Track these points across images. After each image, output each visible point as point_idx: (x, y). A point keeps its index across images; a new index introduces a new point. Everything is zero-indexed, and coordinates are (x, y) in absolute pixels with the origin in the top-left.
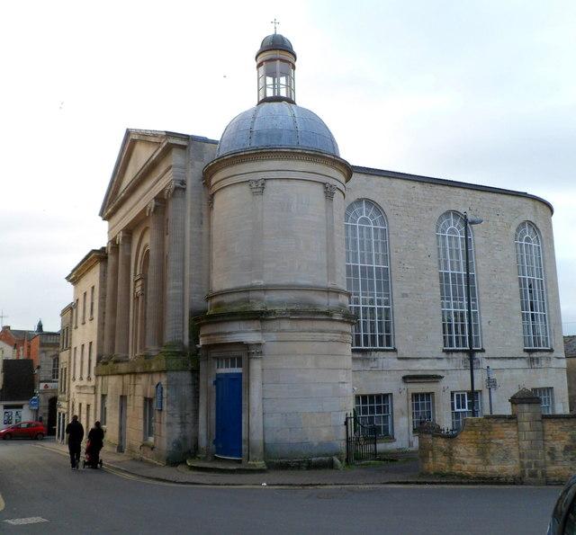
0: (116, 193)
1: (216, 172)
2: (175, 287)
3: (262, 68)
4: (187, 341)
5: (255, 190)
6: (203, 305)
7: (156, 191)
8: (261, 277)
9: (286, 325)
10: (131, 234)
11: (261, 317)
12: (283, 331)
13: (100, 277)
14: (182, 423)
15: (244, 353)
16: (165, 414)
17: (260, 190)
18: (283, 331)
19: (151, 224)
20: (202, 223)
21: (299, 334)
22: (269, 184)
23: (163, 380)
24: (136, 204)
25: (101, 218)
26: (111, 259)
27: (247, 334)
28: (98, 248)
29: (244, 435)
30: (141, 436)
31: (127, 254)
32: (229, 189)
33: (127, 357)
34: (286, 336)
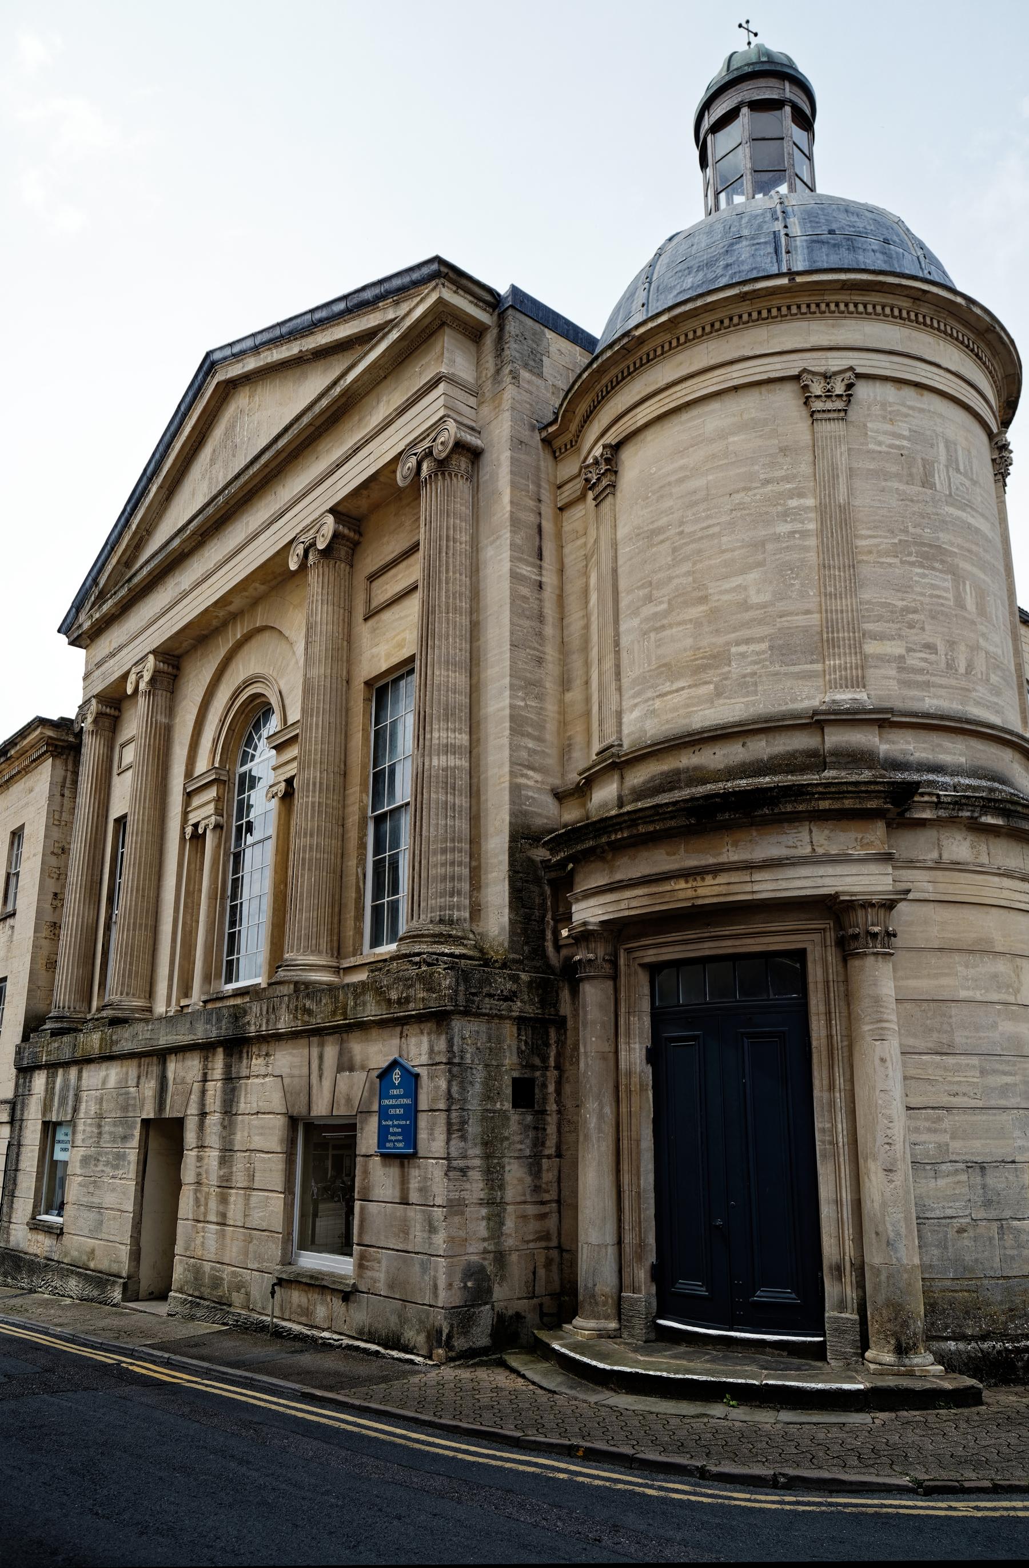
0: (95, 582)
1: (649, 360)
2: (448, 749)
3: (722, 143)
4: (497, 920)
5: (818, 405)
6: (550, 813)
7: (157, 637)
8: (860, 683)
9: (959, 846)
10: (177, 667)
11: (894, 803)
12: (957, 866)
13: (51, 797)
14: (490, 1202)
15: (850, 927)
16: (431, 1175)
17: (839, 404)
18: (957, 866)
19: (315, 582)
20: (540, 556)
21: (996, 879)
22: (863, 391)
23: (419, 1049)
24: (402, 411)
25: (63, 639)
26: (91, 749)
27: (845, 867)
28: (53, 714)
29: (833, 1244)
30: (274, 1250)
31: (162, 719)
32: (650, 435)
33: (150, 1010)
34: (963, 886)
